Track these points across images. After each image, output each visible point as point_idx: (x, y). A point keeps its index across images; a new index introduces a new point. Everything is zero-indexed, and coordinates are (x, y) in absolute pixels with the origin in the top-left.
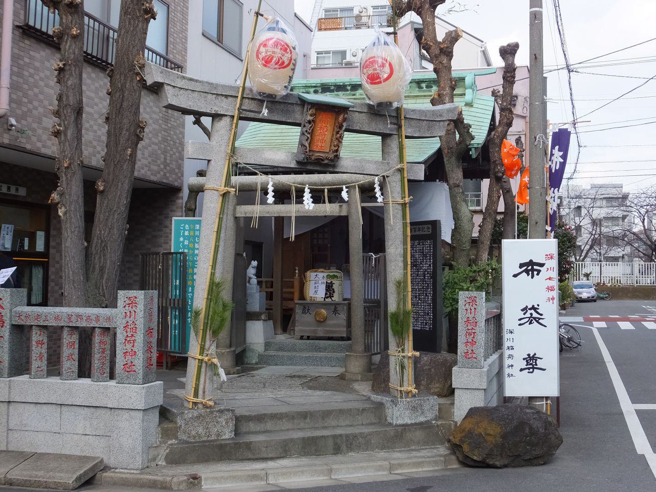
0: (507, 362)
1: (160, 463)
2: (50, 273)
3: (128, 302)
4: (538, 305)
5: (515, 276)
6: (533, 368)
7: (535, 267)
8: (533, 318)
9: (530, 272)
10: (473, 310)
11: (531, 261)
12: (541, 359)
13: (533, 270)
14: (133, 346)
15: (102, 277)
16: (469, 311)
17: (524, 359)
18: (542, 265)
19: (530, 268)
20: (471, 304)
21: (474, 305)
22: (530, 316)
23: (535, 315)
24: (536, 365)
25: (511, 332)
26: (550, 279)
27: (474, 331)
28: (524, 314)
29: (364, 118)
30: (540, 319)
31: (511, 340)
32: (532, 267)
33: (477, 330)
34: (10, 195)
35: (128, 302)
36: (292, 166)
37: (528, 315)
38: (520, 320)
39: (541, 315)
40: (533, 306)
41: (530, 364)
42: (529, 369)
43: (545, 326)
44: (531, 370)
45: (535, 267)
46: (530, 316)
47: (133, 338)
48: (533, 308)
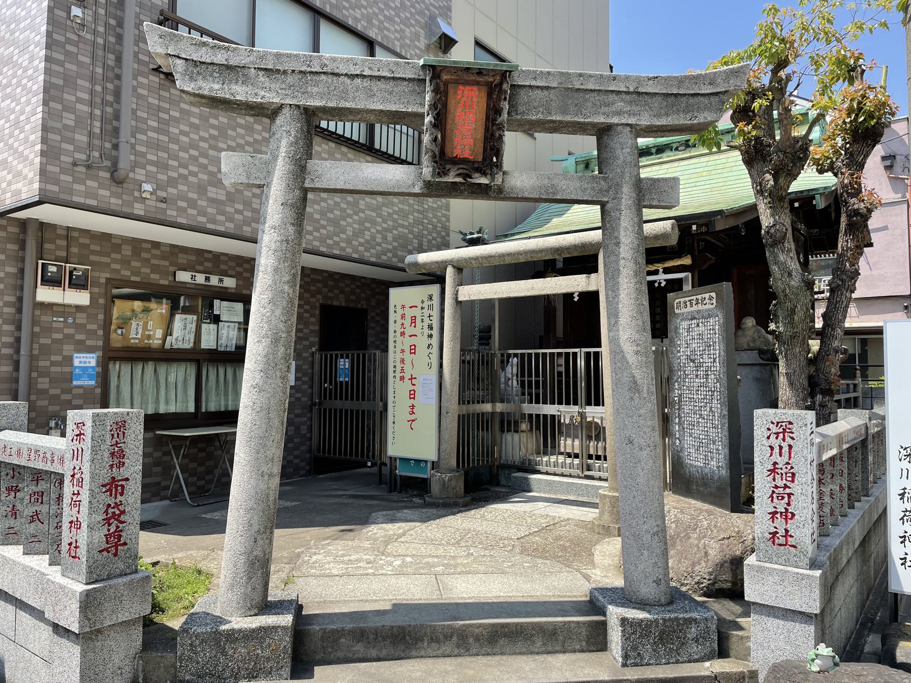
3: (775, 429)
10: (786, 449)
14: (789, 504)
16: (777, 450)
20: (781, 435)
21: (788, 439)
27: (788, 491)
33: (796, 488)
35: (775, 429)
47: (788, 491)
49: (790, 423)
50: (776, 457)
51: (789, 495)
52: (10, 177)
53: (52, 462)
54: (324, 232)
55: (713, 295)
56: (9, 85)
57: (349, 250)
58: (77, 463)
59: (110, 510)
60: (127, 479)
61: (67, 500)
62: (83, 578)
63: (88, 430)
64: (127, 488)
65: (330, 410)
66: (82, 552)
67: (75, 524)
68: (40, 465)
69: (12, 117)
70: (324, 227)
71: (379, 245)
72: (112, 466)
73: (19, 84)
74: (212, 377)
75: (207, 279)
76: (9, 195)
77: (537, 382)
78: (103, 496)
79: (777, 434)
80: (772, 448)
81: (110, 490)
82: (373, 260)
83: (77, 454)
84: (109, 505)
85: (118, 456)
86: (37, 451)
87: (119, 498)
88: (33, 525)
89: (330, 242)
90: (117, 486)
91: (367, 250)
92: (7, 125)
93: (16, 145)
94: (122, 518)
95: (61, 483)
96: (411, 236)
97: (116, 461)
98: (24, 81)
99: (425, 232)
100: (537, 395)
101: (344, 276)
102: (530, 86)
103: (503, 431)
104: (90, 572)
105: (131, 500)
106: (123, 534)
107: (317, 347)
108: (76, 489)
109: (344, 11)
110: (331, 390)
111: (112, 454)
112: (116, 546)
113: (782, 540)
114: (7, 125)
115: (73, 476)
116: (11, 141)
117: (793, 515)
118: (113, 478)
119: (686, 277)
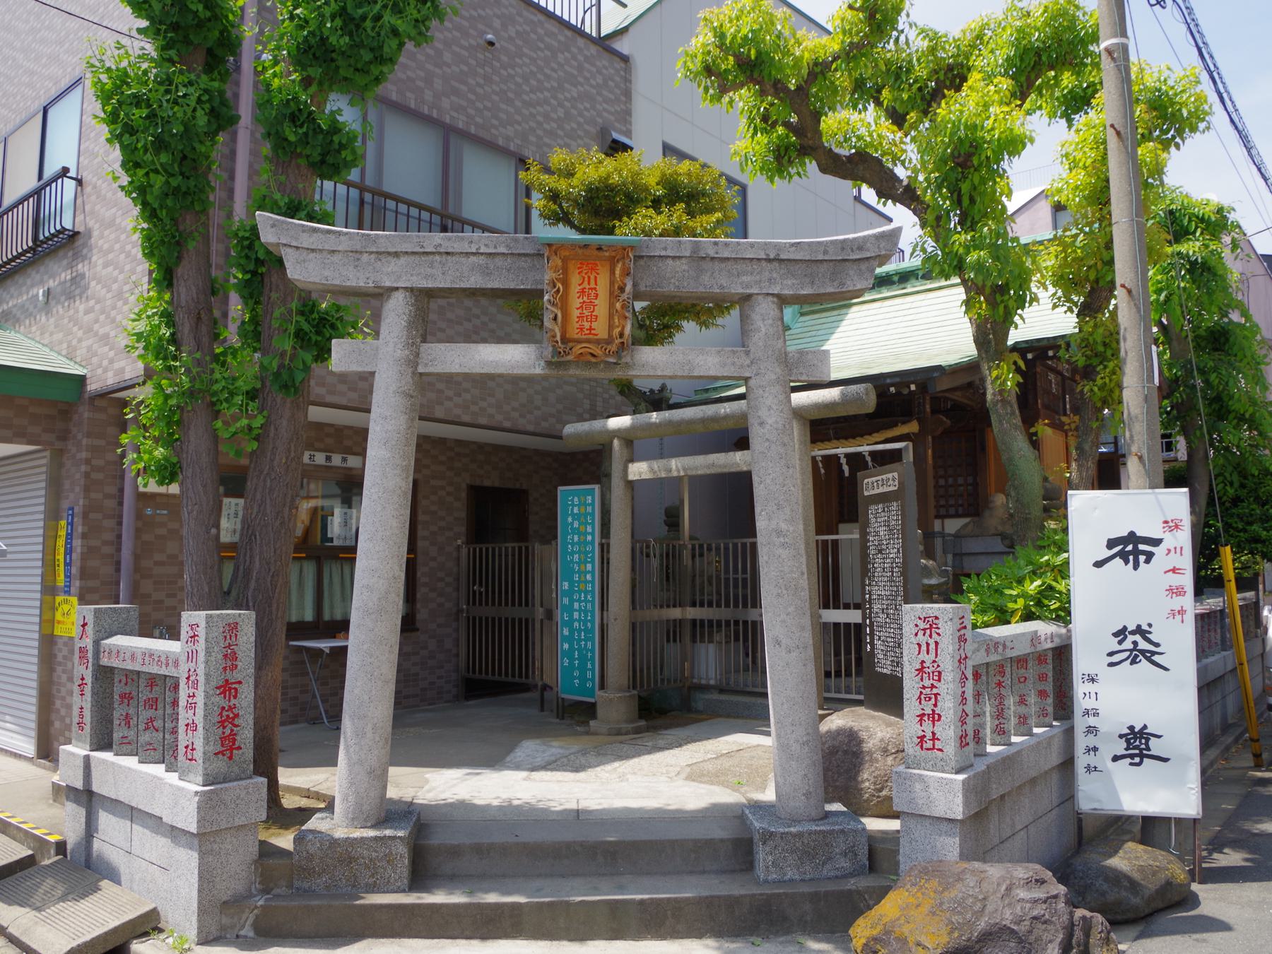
0: (1081, 742)
1: (242, 933)
2: (419, 574)
3: (922, 625)
4: (1150, 625)
5: (1099, 564)
6: (1142, 756)
7: (1141, 547)
8: (1140, 651)
9: (1131, 558)
11: (1132, 534)
12: (1159, 737)
13: (1136, 553)
14: (935, 705)
15: (246, 587)
16: (924, 648)
17: (1121, 736)
18: (1157, 542)
19: (1131, 548)
21: (934, 635)
22: (1131, 646)
23: (1143, 645)
24: (1148, 749)
25: (1093, 680)
26: (1174, 570)
27: (935, 691)
28: (1120, 643)
29: (685, 267)
30: (1154, 653)
31: (1093, 696)
32: (1135, 547)
33: (942, 688)
34: (331, 467)
35: (922, 625)
36: (538, 371)
37: (1128, 644)
38: (1111, 654)
39: (1157, 645)
40: (1139, 627)
41: (1135, 748)
42: (1132, 756)
43: (1166, 669)
44: (1137, 760)
45: (1141, 547)
46: (1131, 646)
47: (935, 691)
48: (1139, 630)
49: (937, 618)
50: (923, 656)
51: (936, 695)
52: (112, 354)
53: (167, 665)
54: (468, 396)
55: (896, 475)
56: (110, 250)
57: (499, 417)
58: (192, 666)
59: (225, 713)
60: (240, 682)
61: (182, 702)
62: (200, 779)
63: (201, 631)
64: (240, 690)
65: (481, 619)
66: (198, 754)
67: (191, 727)
68: (155, 670)
69: (115, 286)
70: (467, 391)
71: (538, 408)
72: (225, 669)
73: (122, 250)
74: (336, 579)
75: (328, 459)
76: (110, 374)
77: (745, 580)
78: (218, 699)
79: (924, 630)
80: (919, 645)
81: (223, 693)
82: (531, 428)
83: (191, 656)
84: (223, 708)
85: (231, 657)
86: (151, 655)
87: (233, 701)
88: (147, 732)
89: (474, 408)
90: (230, 689)
91: (522, 416)
92: (109, 295)
93: (119, 318)
94: (236, 722)
95: (176, 687)
96: (580, 396)
97: (229, 663)
98: (128, 247)
99: (599, 390)
100: (745, 597)
101: (497, 448)
102: (661, 257)
103: (694, 641)
104: (206, 775)
105: (244, 704)
106: (238, 738)
107: (464, 538)
108: (191, 691)
109: (493, 131)
110: (481, 593)
111: (225, 656)
112: (231, 749)
113: (929, 744)
114: (109, 295)
115: (188, 678)
116: (113, 313)
117: (940, 716)
118: (227, 681)
119: (906, 447)
